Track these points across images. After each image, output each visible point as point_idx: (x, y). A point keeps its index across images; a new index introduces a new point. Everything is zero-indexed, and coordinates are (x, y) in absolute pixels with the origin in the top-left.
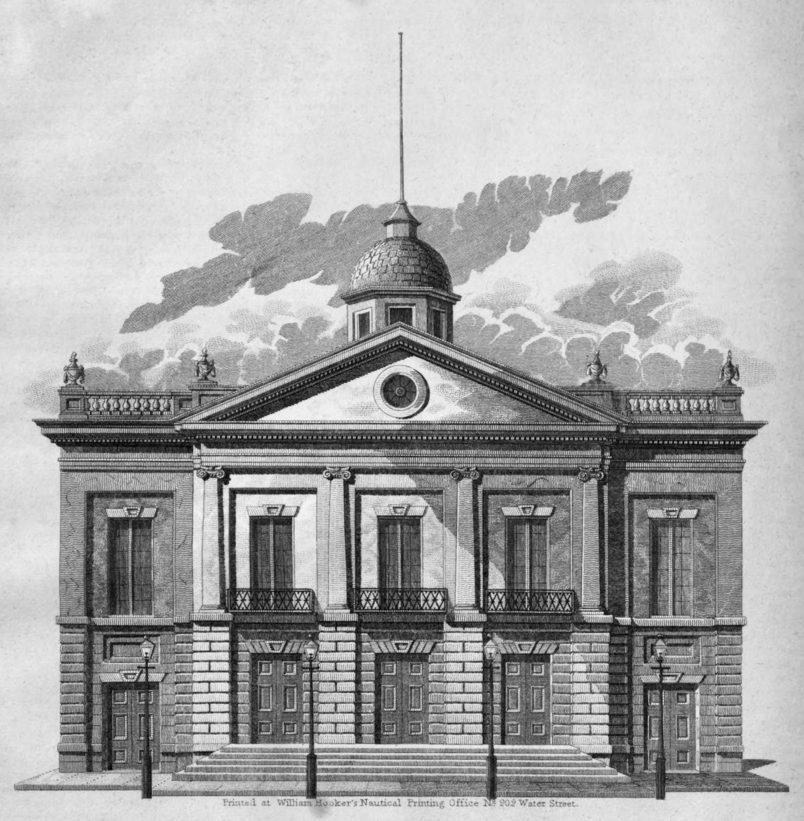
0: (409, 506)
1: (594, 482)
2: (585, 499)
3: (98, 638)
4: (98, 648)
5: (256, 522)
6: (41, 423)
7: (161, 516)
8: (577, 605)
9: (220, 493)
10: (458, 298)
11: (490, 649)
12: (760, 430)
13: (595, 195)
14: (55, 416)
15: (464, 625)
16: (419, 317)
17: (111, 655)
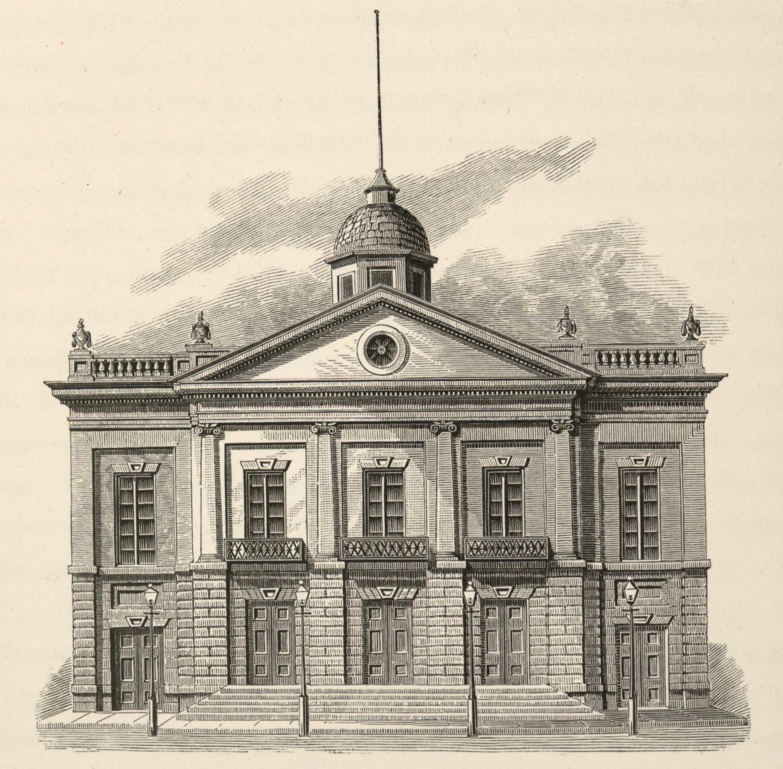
0: (392, 459)
1: (566, 433)
3: (106, 587)
4: (106, 596)
6: (53, 386)
7: (162, 471)
8: (552, 554)
9: (217, 450)
10: (435, 260)
11: (470, 595)
12: (720, 383)
13: (558, 159)
14: (64, 378)
16: (398, 280)
17: (119, 603)
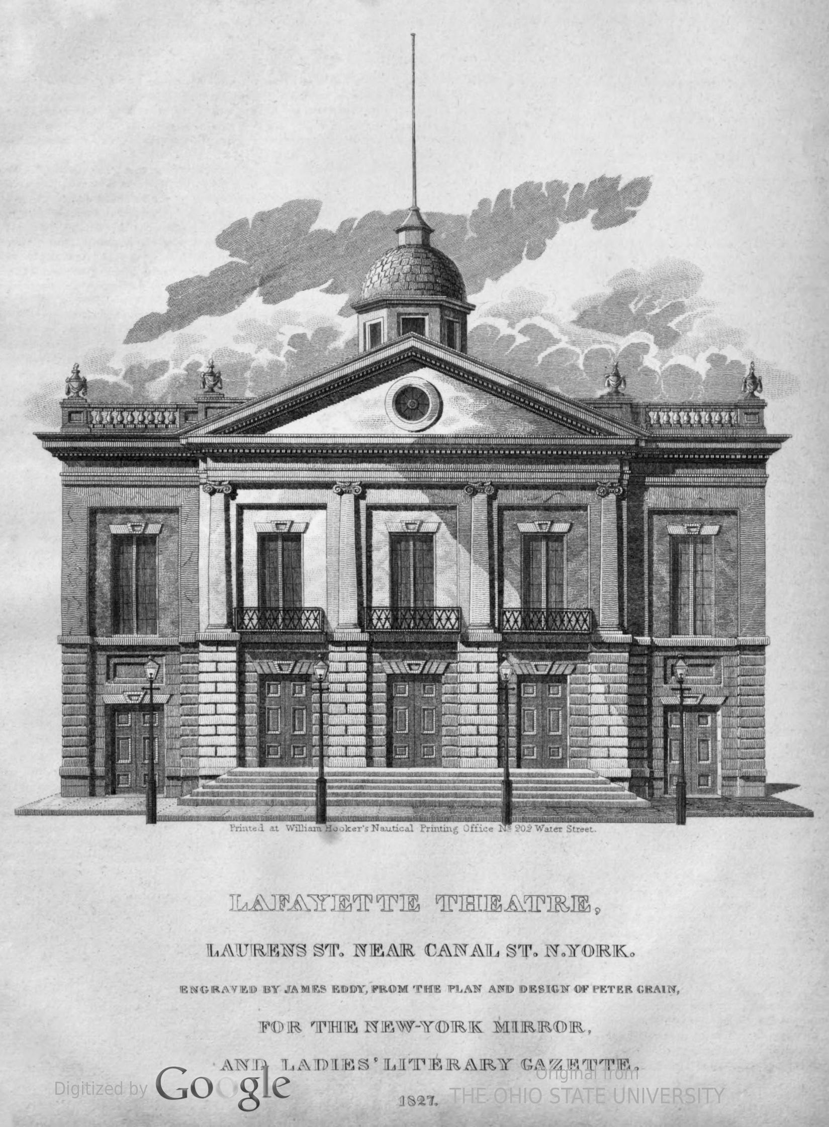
0: (422, 522)
1: (612, 497)
2: (603, 515)
3: (101, 658)
4: (101, 669)
5: (264, 539)
6: (42, 437)
7: (166, 532)
8: (595, 624)
9: (227, 509)
10: (472, 308)
11: (506, 670)
12: (783, 444)
13: (613, 201)
14: (57, 429)
15: (479, 644)
16: (433, 327)
17: (115, 675)
